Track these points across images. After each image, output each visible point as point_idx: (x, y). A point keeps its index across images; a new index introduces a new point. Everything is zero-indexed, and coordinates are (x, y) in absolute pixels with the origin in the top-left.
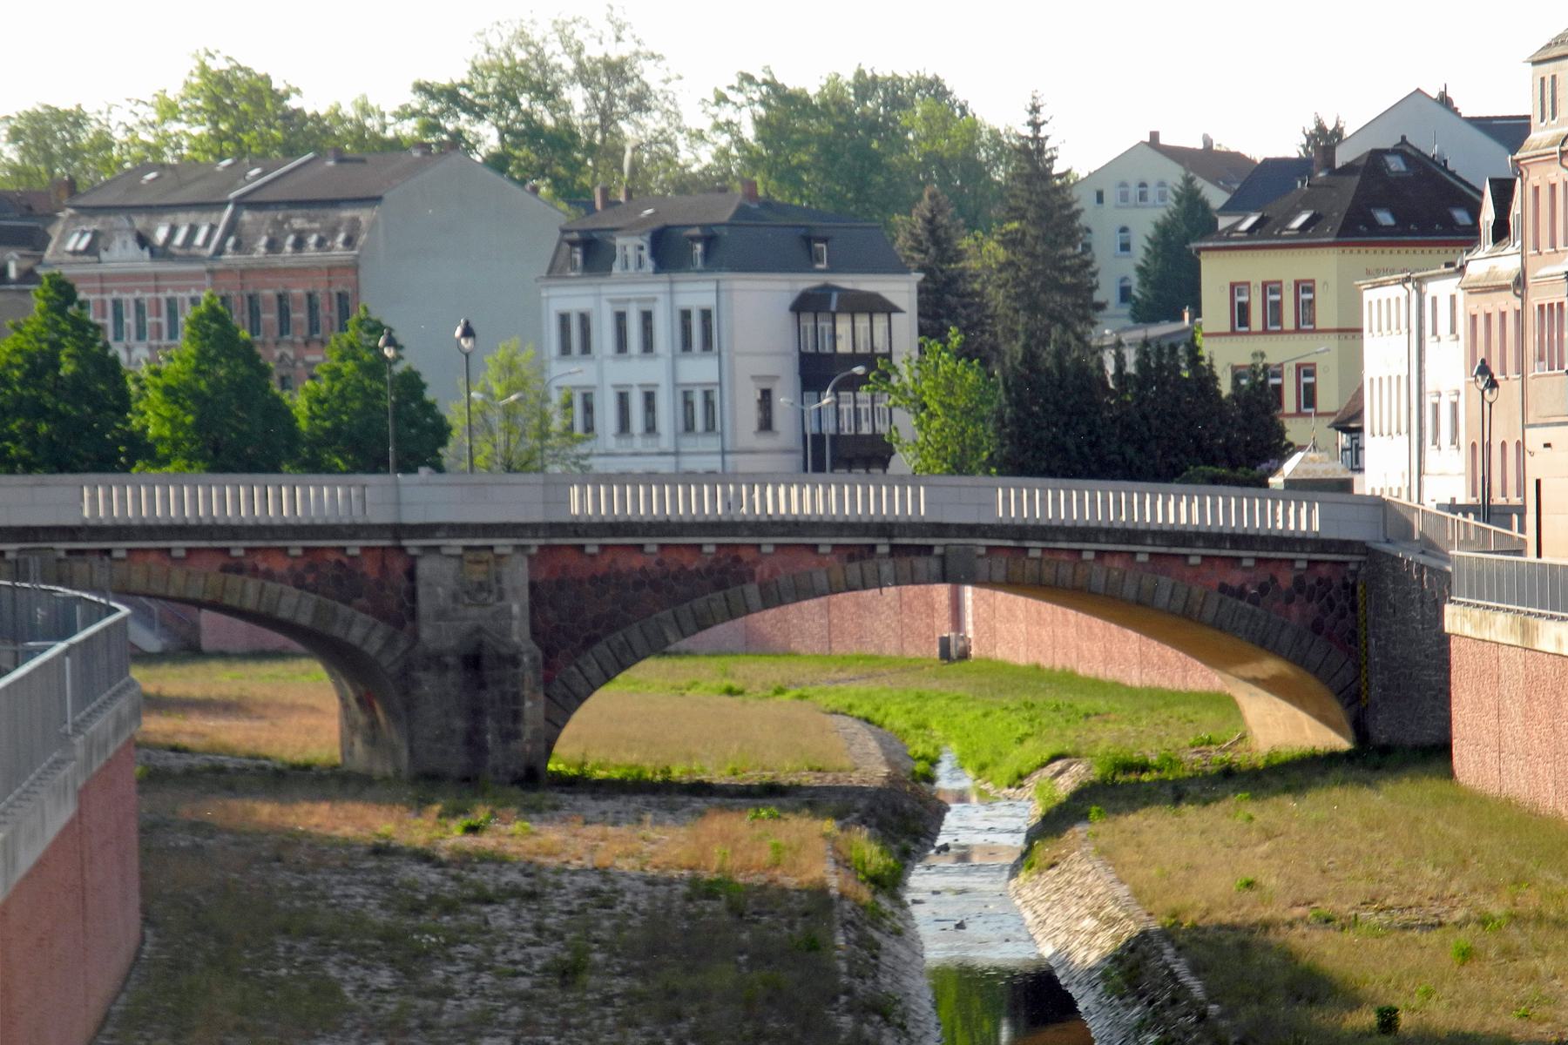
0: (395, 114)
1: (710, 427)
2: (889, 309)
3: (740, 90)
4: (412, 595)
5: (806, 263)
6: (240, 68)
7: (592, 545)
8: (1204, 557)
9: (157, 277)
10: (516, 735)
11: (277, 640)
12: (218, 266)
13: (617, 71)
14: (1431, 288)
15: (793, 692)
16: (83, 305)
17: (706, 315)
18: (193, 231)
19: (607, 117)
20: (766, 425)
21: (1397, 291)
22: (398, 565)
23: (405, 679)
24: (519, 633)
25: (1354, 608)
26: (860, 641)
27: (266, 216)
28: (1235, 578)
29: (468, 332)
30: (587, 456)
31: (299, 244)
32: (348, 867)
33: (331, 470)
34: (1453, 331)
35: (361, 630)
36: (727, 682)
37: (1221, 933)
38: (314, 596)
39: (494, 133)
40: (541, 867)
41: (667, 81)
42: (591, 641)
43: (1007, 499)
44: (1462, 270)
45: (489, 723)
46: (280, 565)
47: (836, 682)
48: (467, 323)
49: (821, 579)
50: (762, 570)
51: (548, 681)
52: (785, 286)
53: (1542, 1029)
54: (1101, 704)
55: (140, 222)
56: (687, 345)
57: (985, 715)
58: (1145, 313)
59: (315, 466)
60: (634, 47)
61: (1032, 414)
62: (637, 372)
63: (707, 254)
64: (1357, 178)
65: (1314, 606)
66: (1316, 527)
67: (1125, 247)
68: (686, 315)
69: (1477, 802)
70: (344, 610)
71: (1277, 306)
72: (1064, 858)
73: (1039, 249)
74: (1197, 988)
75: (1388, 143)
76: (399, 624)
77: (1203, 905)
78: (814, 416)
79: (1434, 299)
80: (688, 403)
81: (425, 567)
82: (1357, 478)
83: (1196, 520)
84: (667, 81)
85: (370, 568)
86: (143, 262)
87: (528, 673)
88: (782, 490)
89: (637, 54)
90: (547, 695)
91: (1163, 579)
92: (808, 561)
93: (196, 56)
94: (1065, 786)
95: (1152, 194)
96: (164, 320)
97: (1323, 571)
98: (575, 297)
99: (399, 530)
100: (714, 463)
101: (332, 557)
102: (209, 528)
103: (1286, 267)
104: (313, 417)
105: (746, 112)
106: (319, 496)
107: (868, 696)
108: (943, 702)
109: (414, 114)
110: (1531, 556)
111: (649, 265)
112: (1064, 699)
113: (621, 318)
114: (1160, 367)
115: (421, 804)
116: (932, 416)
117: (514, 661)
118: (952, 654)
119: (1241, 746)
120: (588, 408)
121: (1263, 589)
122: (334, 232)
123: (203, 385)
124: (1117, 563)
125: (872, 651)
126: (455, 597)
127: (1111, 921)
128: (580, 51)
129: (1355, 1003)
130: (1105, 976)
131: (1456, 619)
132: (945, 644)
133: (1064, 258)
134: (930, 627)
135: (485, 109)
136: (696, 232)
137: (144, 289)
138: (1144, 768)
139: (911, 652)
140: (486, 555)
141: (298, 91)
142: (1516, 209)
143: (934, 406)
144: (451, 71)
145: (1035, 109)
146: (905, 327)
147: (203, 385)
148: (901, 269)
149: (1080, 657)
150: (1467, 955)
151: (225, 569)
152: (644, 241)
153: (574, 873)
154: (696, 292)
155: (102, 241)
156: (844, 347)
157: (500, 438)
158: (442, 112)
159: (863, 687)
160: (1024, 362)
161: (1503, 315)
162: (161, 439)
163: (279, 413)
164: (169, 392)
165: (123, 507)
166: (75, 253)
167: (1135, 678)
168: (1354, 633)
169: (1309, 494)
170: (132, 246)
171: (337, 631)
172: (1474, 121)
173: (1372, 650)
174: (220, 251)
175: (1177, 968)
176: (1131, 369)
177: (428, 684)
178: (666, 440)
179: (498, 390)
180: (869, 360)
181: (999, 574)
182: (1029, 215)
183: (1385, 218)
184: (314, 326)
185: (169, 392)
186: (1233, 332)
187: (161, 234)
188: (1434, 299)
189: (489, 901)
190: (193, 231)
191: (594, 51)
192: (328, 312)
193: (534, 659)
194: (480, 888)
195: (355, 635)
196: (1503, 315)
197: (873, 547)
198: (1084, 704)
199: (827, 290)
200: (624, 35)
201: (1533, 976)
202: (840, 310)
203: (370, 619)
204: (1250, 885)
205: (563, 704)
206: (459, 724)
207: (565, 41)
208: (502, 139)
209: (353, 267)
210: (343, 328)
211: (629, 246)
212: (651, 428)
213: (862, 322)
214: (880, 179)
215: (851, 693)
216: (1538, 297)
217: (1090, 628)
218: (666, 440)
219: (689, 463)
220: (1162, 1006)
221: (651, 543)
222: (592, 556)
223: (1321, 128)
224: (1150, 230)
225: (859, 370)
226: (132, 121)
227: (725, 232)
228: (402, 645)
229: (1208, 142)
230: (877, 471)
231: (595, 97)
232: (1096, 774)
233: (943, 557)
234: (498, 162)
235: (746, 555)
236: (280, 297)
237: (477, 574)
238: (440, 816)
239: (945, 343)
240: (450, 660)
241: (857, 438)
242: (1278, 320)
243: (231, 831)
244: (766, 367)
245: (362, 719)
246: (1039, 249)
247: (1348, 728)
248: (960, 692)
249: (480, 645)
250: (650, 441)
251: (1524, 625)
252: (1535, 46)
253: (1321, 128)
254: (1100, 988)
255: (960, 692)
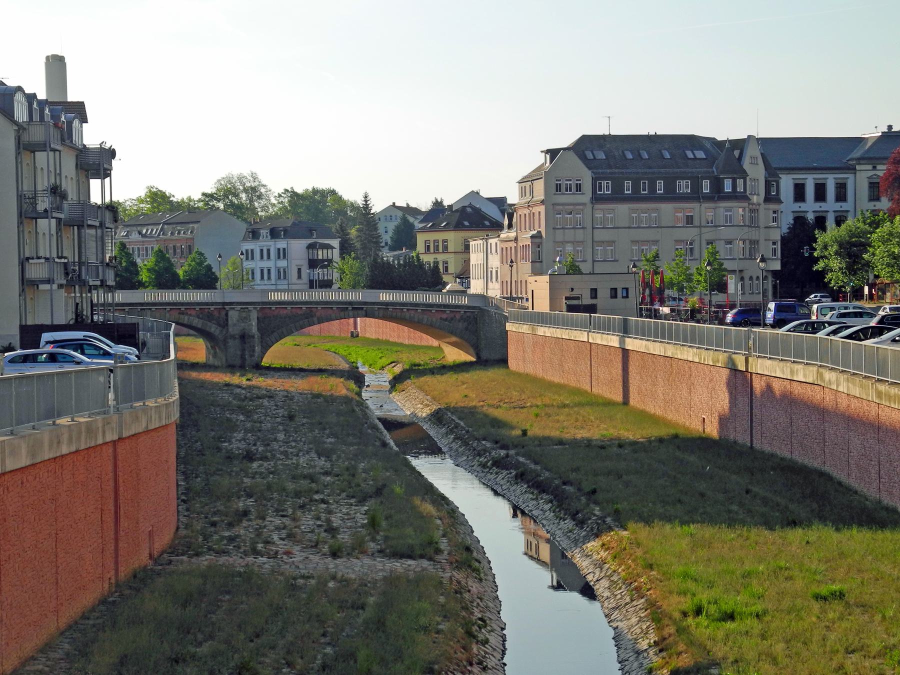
0: (197, 201)
1: (285, 278)
2: (332, 248)
3: (285, 194)
4: (227, 320)
5: (310, 236)
6: (159, 190)
7: (273, 307)
8: (436, 311)
9: (143, 242)
10: (254, 356)
11: (192, 332)
12: (159, 239)
13: (254, 189)
14: (490, 241)
15: (313, 345)
16: (128, 249)
17: (284, 249)
18: (152, 230)
19: (251, 201)
20: (299, 277)
21: (481, 242)
22: (223, 313)
23: (225, 342)
24: (254, 330)
25: (477, 324)
26: (329, 332)
27: (171, 226)
28: (444, 316)
29: (220, 256)
30: (253, 285)
31: (179, 233)
32: (220, 389)
33: (189, 289)
34: (496, 252)
35: (213, 329)
36: (295, 343)
37: (462, 409)
38: (202, 320)
39: (222, 205)
40: (270, 390)
41: (267, 192)
42: (273, 332)
43: (271, 295)
44: (499, 236)
45: (247, 353)
46: (193, 312)
47: (324, 343)
48: (762, 256)
49: (333, 316)
50: (318, 314)
51: (262, 342)
52: (305, 242)
53: (568, 435)
54: (399, 349)
55: (139, 228)
56: (279, 257)
57: (368, 351)
58: (396, 246)
59: (184, 288)
60: (258, 183)
61: (375, 274)
62: (265, 264)
63: (284, 235)
64: (459, 214)
65: (466, 324)
66: (466, 303)
67: (386, 232)
68: (279, 249)
69: (518, 375)
70: (209, 324)
71: (438, 246)
72: (407, 388)
73: (367, 232)
74: (462, 423)
75: (467, 204)
76: (224, 327)
77: (455, 401)
78: (317, 274)
79: (491, 244)
80: (279, 272)
81: (231, 313)
82: (468, 290)
83: (388, 299)
84: (267, 192)
85: (216, 313)
86: (140, 238)
87: (257, 340)
88: (279, 293)
89: (259, 185)
90: (261, 346)
91: (425, 316)
92: (330, 312)
93: (148, 188)
94: (398, 369)
95: (393, 218)
96: (144, 252)
97: (468, 314)
98: (248, 246)
99: (224, 304)
100: (286, 287)
101: (206, 310)
102: (175, 303)
103: (440, 236)
104: (184, 276)
105: (287, 199)
106: (204, 295)
107: (333, 346)
108: (354, 348)
109: (202, 201)
110: (530, 310)
111: (269, 237)
112: (389, 348)
113: (262, 251)
114: (409, 261)
115: (233, 373)
116: (347, 275)
117: (253, 337)
118: (354, 335)
119: (443, 360)
120: (253, 273)
121: (452, 319)
122: (188, 230)
123: (157, 268)
124: (413, 312)
125: (332, 335)
126: (238, 321)
127: (427, 406)
128: (245, 184)
129: (512, 428)
130: (430, 420)
131: (509, 326)
132: (352, 333)
133: (373, 235)
134: (348, 329)
135: (220, 199)
136: (282, 229)
137: (140, 245)
138: (420, 365)
139: (343, 335)
140: (246, 310)
141: (173, 196)
142: (514, 220)
143: (347, 272)
144: (210, 190)
145: (366, 197)
146: (336, 252)
147: (157, 268)
148: (334, 237)
149: (391, 336)
150: (537, 415)
151: (179, 313)
152: (268, 231)
153: (279, 391)
154: (282, 244)
155: (129, 234)
156: (320, 257)
157: (232, 281)
158: (209, 200)
159: (332, 344)
160: (373, 260)
161: (511, 248)
162: (146, 282)
163: (176, 275)
164: (149, 270)
165: (274, 297)
166: (123, 236)
167: (406, 342)
168: (477, 330)
169: (459, 294)
170: (137, 234)
171: (208, 329)
172: (486, 198)
173: (482, 335)
174: (159, 235)
175: (454, 418)
176: (402, 262)
177: (231, 343)
178: (273, 282)
179: (231, 269)
180: (327, 260)
181: (381, 315)
182: (365, 224)
183: (466, 223)
184: (182, 254)
185: (149, 270)
186: (426, 253)
187: (144, 231)
188: (491, 244)
189: (260, 398)
190: (152, 230)
191: (248, 184)
192: (186, 251)
193: (258, 336)
194: (257, 395)
195: (213, 330)
196: (511, 248)
197: (347, 308)
198: (395, 349)
199: (316, 243)
200: (256, 181)
201: (558, 421)
202: (319, 248)
203: (216, 326)
204: (466, 396)
205: (266, 348)
206: (239, 353)
207: (241, 182)
208: (224, 206)
209: (193, 239)
210: (190, 253)
211: (264, 232)
212: (269, 278)
213: (325, 251)
214: (321, 215)
215: (328, 346)
216: (520, 244)
217: (403, 330)
218: (273, 282)
219: (279, 287)
220: (452, 428)
221: (289, 307)
222: (273, 310)
223: (437, 201)
224: (394, 227)
225: (326, 263)
226: (131, 204)
227: (289, 229)
228: (224, 333)
229: (408, 204)
230: (329, 289)
231: (248, 196)
232: (407, 367)
233: (366, 310)
234: (225, 211)
235: (314, 310)
236: (174, 246)
237: (244, 315)
238: (240, 376)
239: (350, 255)
240: (237, 336)
241: (324, 281)
242: (438, 250)
243: (187, 379)
244: (299, 262)
245: (212, 351)
246: (367, 232)
247: (475, 357)
248: (359, 345)
249: (244, 333)
250: (269, 281)
251: (532, 328)
252: (519, 178)
253: (437, 201)
254: (429, 423)
255: (359, 345)
